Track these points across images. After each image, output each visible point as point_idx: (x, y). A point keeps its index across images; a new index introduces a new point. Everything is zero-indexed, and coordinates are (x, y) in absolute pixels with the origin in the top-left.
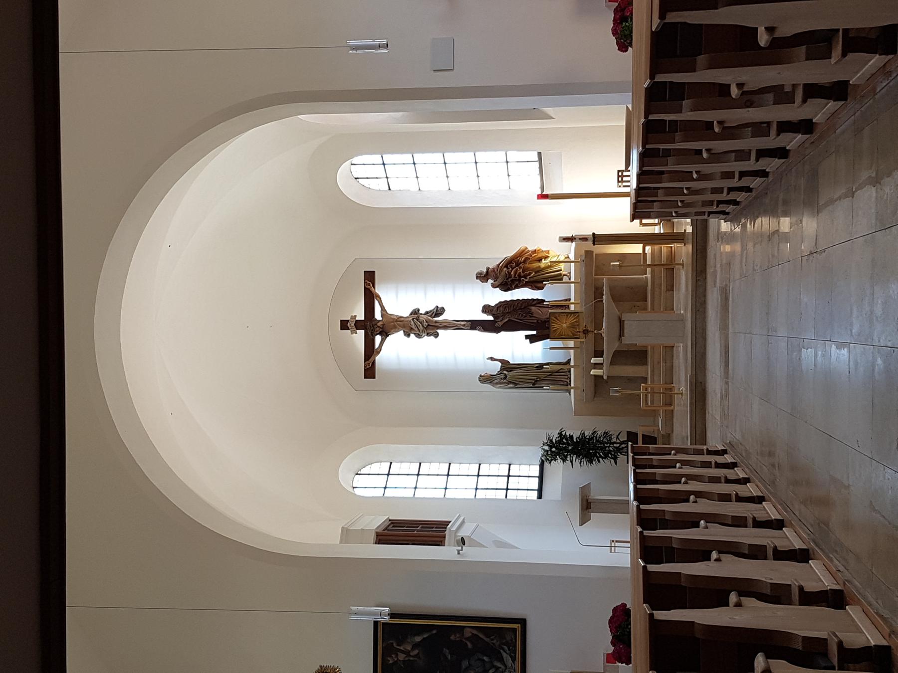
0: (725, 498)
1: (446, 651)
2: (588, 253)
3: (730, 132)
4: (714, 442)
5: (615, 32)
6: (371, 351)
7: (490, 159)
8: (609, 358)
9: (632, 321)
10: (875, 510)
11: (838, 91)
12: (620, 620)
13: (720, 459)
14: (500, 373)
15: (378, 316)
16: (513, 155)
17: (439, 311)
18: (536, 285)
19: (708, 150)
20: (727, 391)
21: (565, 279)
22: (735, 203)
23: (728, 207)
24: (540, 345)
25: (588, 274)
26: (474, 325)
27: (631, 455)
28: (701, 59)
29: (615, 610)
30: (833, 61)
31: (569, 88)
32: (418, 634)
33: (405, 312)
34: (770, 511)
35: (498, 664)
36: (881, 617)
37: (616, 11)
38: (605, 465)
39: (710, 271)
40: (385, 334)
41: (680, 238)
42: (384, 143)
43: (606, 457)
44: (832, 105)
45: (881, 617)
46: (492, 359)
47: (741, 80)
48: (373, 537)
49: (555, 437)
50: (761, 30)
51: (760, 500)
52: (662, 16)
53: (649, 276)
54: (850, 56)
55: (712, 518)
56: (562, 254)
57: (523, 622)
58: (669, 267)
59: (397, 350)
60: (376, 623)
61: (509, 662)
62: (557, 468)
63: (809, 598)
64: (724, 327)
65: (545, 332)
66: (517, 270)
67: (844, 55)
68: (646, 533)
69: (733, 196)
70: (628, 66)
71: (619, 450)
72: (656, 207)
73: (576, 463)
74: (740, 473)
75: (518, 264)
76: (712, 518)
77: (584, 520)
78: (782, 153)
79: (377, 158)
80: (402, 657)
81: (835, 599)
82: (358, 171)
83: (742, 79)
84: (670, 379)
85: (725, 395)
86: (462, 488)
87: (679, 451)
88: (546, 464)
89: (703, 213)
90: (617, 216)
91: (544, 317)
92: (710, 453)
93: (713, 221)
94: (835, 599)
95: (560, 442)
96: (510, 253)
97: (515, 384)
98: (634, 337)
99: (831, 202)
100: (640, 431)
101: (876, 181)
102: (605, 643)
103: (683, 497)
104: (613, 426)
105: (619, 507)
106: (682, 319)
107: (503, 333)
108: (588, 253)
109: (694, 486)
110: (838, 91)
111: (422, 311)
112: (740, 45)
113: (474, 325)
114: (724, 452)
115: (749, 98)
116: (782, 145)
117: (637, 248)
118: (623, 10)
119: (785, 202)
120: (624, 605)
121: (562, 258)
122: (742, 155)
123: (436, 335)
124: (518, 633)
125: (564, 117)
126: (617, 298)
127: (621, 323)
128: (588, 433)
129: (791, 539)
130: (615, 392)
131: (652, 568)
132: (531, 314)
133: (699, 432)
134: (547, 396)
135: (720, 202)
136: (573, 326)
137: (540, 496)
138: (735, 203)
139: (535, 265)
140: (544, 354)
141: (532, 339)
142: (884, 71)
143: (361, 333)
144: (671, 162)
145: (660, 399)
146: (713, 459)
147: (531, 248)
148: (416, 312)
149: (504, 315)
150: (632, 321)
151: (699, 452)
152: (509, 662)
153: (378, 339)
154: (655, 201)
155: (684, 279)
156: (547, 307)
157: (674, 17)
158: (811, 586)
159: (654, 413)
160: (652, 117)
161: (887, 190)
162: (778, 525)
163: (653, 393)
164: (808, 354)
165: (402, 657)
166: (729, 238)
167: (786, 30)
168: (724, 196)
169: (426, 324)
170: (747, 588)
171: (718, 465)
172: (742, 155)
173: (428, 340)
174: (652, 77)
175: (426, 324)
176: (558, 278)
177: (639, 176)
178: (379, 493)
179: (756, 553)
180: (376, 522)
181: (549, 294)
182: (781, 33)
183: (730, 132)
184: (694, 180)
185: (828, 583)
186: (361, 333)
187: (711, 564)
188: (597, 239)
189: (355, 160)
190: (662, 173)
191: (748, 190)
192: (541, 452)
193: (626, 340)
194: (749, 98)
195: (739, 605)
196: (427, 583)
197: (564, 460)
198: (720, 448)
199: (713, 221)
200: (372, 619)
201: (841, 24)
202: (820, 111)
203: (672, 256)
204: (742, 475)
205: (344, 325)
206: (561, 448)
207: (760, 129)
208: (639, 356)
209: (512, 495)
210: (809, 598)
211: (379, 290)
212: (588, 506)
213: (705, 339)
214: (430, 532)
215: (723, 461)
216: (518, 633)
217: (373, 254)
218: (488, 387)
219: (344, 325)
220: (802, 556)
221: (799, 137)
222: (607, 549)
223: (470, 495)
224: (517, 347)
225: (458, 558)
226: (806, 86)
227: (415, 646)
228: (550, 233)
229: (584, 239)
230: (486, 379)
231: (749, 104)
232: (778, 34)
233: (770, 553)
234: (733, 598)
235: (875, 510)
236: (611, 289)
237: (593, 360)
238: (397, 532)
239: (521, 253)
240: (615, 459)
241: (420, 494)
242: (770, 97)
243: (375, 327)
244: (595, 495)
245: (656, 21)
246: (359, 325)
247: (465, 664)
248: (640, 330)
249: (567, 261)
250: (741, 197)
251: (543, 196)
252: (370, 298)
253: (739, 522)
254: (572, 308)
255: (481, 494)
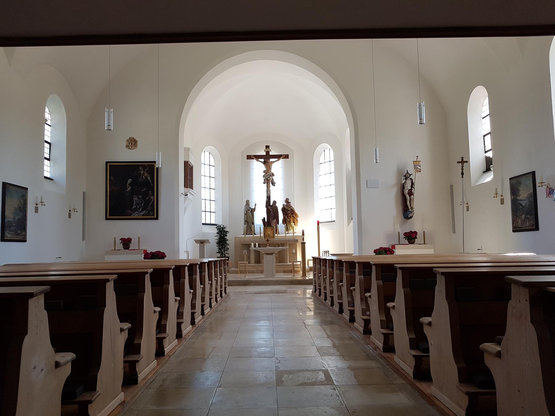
0: (211, 294)
1: (145, 189)
2: (297, 241)
3: (350, 293)
4: (229, 289)
5: (381, 248)
6: (257, 157)
7: (333, 203)
8: (258, 248)
9: (273, 258)
10: (213, 349)
11: (367, 331)
12: (160, 255)
13: (223, 292)
14: (250, 208)
15: (271, 160)
16: (334, 211)
17: (273, 184)
18: (284, 221)
19: (342, 285)
20: (249, 294)
21: (287, 232)
22: (320, 295)
23: (318, 293)
24: (262, 223)
25: (289, 241)
26: (269, 198)
27: (223, 259)
28: (381, 282)
29: (164, 253)
30: (380, 330)
31: (361, 232)
32: (151, 178)
33: (273, 171)
34: (207, 310)
35: (141, 209)
36: (174, 352)
37: (389, 248)
38: (216, 249)
39: (292, 286)
40: (265, 163)
41: (304, 275)
42: (338, 161)
43: (219, 249)
44: (361, 329)
45: (174, 352)
46: (256, 205)
47: (372, 297)
48: (187, 160)
49: (226, 230)
50: (393, 304)
51: (211, 307)
52: (400, 268)
53: (289, 264)
54: (382, 336)
55: (204, 289)
56: (297, 230)
57: (157, 218)
58: (293, 271)
59: (258, 167)
60: (155, 162)
61: (142, 213)
62: (214, 230)
63: (179, 325)
64: (272, 292)
65: (266, 225)
66: (290, 213)
67: (383, 334)
68: (198, 266)
69: (323, 294)
70: (368, 253)
71: (222, 253)
72: (318, 266)
73: (217, 238)
74: (219, 299)
75: (292, 214)
76: (204, 289)
77: (196, 241)
78: (341, 311)
79: (332, 159)
80: (142, 172)
81: (179, 335)
82: (327, 151)
83: (373, 297)
84: (253, 272)
85: (246, 293)
86: (205, 194)
87: (225, 276)
88: (216, 226)
89: (315, 283)
90: (311, 252)
91: (272, 224)
92: (225, 288)
93: (312, 287)
94: (179, 335)
95: (224, 232)
96: (296, 211)
97: (246, 214)
98: (267, 259)
99: (325, 330)
100: (230, 262)
101: (334, 346)
102: (151, 249)
103: (210, 279)
104: (231, 251)
105: (202, 255)
106: (273, 276)
107: (266, 209)
108: (297, 241)
109: (214, 283)
110: (367, 331)
111: (273, 177)
112: (387, 296)
113: (269, 198)
114: (226, 293)
115: (365, 300)
116: (344, 311)
117: (299, 258)
118: (389, 251)
119: (320, 313)
120: (165, 256)
121: (295, 231)
122: (340, 297)
123: (264, 183)
124: (153, 217)
125: (349, 230)
126: (280, 252)
127: (272, 254)
128: (228, 242)
129: (198, 318)
130: (245, 252)
131: (186, 268)
132: (273, 219)
133: (232, 283)
134: (242, 226)
135: (320, 289)
136: (269, 235)
137: (203, 224)
138: (320, 295)
139: (292, 221)
140: (258, 225)
141: (264, 220)
142: (376, 348)
143: (265, 154)
144: (334, 272)
145: (242, 269)
146: (223, 289)
147: (298, 219)
148: (273, 175)
149: (273, 209)
150: (273, 258)
151: (225, 284)
152: (142, 213)
153: (262, 160)
154: (320, 265)
155: (288, 277)
156: (276, 226)
157: (399, 272)
158: (183, 326)
159: (237, 266)
160: (357, 265)
161: (332, 350)
162: (203, 314)
163: (245, 266)
164: (262, 323)
165: (142, 172)
166: (305, 293)
167: (393, 313)
168: (322, 291)
169: (268, 179)
170: (181, 303)
171: (221, 291)
172: (340, 297)
173: (262, 180)
174: (374, 265)
175: (268, 179)
176: (287, 229)
177: (332, 260)
178: (203, 162)
179: (193, 306)
180: (192, 162)
181: (281, 226)
182: (392, 311)
183: (350, 293)
184: (330, 280)
185: (184, 332)
186: (265, 154)
187: (189, 290)
188: (303, 244)
189: (331, 150)
190: (326, 267)
191: (326, 299)
192: (220, 224)
193: (265, 256)
194: (365, 300)
195: (176, 300)
196: (170, 181)
197: (218, 233)
198: (227, 291)
199: (312, 287)
200: (157, 160)
201: (395, 332)
202: (359, 325)
203: (297, 272)
204: (218, 300)
205: (267, 147)
206: (222, 232)
207: (352, 304)
208: (258, 260)
209: (203, 213)
210: (179, 325)
211: (281, 160)
212: (202, 242)
213: (267, 285)
214: (189, 182)
215: (223, 292)
216: (153, 217)
217: (295, 158)
218: (245, 203)
219: (267, 147)
220: (193, 323)
221: (348, 318)
222: (185, 251)
223: (203, 197)
224: (260, 215)
225: (180, 193)
226: (369, 320)
227: (146, 177)
228: (304, 226)
229: (303, 239)
230: (248, 203)
231: (362, 300)
232: (391, 310)
233: (193, 311)
234: (178, 298)
235: (213, 349)
236: (284, 250)
237: (257, 244)
238: (189, 169)
239: (296, 215)
240: (219, 252)
241: (203, 178)
242: (365, 307)
243: (267, 159)
244: (206, 245)
245: (398, 266)
246: (268, 153)
247: (140, 197)
248: (269, 261)
249: (294, 233)
250: (323, 297)
251: (318, 223)
252: (278, 157)
253: (203, 299)
254: (276, 235)
255: (203, 201)
